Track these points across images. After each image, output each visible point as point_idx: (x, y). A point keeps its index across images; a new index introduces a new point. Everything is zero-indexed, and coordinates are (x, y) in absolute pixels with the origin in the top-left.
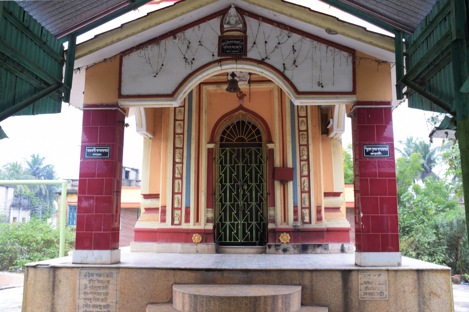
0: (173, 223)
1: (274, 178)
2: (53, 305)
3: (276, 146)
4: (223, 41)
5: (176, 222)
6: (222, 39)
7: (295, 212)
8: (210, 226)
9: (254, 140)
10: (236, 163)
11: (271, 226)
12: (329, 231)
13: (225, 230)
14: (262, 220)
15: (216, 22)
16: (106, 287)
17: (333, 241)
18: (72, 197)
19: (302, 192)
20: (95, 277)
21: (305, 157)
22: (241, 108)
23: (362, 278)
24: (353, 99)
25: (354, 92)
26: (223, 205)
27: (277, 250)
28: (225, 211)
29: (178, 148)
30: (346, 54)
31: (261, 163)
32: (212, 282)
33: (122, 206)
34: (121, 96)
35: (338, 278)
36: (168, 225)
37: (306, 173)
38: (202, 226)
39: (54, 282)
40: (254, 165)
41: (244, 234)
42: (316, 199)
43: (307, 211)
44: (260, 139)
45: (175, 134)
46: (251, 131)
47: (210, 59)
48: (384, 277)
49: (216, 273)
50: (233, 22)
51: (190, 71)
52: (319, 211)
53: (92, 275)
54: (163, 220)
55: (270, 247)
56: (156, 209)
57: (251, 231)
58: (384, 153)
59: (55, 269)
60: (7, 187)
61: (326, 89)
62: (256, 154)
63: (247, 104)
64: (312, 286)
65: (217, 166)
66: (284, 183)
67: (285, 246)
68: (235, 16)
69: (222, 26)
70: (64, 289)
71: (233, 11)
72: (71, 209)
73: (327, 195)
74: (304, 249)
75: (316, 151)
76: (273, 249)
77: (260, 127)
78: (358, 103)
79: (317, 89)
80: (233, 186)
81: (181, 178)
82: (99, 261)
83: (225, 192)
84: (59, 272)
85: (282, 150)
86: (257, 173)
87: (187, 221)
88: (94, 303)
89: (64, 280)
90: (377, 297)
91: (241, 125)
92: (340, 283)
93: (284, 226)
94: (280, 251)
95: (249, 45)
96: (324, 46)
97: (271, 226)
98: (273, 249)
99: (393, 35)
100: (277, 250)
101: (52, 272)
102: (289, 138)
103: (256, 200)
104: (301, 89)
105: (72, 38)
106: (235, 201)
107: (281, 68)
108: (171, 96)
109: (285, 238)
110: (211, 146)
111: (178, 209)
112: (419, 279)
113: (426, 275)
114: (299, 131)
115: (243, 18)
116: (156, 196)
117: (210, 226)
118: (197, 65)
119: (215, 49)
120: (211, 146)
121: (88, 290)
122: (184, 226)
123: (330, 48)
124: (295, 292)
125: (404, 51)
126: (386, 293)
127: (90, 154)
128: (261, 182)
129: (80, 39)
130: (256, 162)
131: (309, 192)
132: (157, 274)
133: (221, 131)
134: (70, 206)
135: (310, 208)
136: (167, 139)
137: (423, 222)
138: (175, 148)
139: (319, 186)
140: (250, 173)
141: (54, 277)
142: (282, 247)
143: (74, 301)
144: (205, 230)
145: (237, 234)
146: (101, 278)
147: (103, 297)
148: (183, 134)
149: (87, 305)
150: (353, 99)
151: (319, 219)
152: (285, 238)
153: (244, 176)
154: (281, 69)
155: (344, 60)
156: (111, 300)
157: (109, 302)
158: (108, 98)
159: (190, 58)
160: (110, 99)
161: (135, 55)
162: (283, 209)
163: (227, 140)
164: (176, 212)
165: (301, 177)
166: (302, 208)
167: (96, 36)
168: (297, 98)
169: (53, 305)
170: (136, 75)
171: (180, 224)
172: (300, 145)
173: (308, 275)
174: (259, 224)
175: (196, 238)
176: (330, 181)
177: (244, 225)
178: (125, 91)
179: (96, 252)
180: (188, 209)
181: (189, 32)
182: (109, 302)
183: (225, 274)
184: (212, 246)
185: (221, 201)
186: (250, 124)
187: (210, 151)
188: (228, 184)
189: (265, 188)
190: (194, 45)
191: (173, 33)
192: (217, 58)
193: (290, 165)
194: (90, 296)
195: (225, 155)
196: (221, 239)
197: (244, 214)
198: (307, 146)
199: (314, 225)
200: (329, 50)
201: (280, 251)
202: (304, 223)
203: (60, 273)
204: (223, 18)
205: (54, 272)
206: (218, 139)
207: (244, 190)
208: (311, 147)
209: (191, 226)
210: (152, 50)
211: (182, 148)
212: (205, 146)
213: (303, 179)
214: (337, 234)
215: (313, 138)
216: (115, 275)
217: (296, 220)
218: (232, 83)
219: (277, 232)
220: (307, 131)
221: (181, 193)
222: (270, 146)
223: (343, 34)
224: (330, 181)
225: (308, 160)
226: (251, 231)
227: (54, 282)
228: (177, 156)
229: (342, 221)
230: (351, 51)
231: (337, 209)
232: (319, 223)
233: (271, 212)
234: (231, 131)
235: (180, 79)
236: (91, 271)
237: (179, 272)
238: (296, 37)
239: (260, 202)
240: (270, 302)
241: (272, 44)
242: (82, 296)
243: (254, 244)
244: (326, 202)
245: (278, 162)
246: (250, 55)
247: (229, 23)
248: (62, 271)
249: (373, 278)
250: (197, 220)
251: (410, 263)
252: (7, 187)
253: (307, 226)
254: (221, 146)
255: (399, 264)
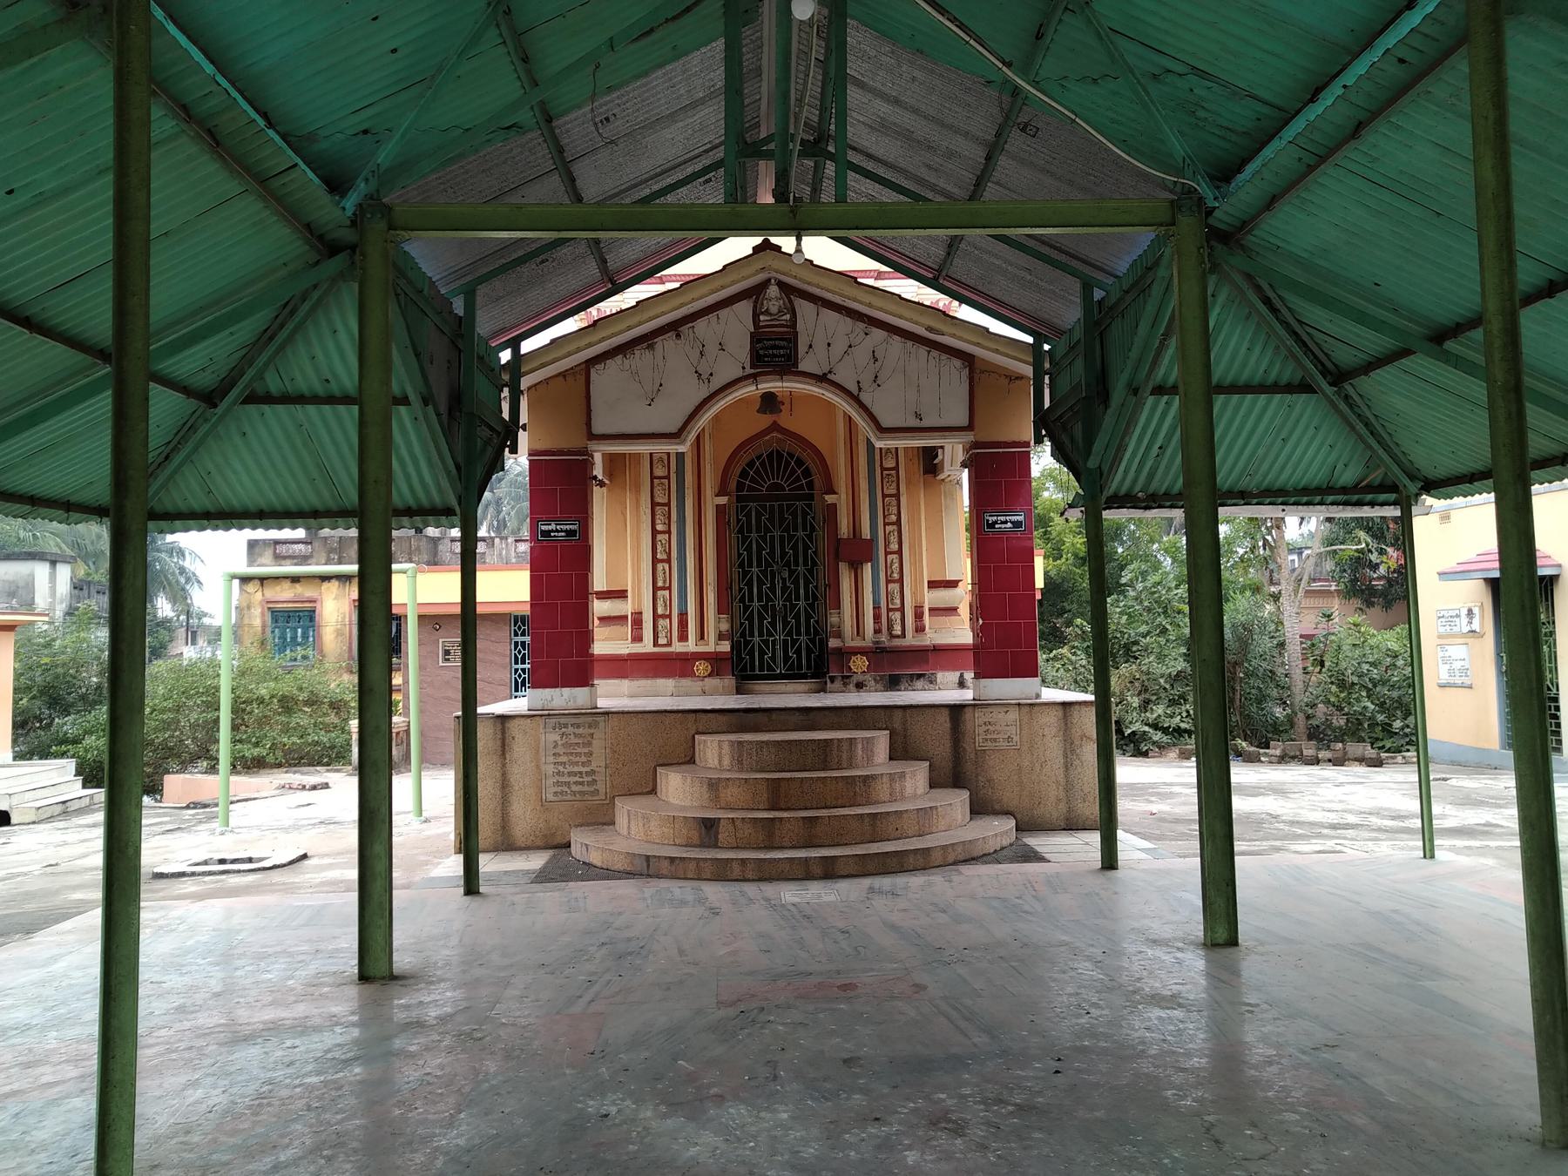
0: (656, 644)
1: (837, 558)
2: (504, 774)
3: (841, 499)
4: (759, 341)
5: (662, 641)
6: (756, 338)
7: (877, 617)
8: (725, 647)
9: (801, 487)
10: (767, 530)
11: (833, 643)
12: (937, 649)
13: (751, 653)
14: (816, 633)
15: (744, 308)
16: (589, 744)
17: (945, 668)
18: (278, 588)
19: (888, 582)
20: (570, 730)
21: (894, 518)
22: (775, 427)
23: (980, 717)
24: (970, 437)
25: (970, 427)
26: (746, 608)
27: (845, 684)
28: (750, 619)
29: (659, 504)
30: (957, 363)
31: (813, 529)
32: (756, 729)
33: (480, 610)
34: (592, 437)
35: (944, 718)
36: (647, 646)
37: (894, 547)
38: (711, 646)
39: (503, 740)
40: (801, 533)
41: (786, 658)
42: (914, 594)
43: (898, 615)
44: (810, 485)
45: (653, 478)
46: (793, 472)
47: (740, 373)
48: (1013, 715)
49: (759, 715)
50: (774, 310)
51: (704, 394)
52: (919, 615)
53: (566, 726)
54: (637, 638)
55: (832, 680)
56: (622, 619)
57: (798, 652)
58: (1017, 524)
59: (503, 719)
60: (53, 563)
61: (926, 423)
62: (805, 514)
63: (785, 420)
64: (905, 730)
65: (732, 537)
66: (856, 567)
67: (861, 678)
68: (778, 299)
69: (756, 316)
70: (520, 749)
71: (773, 291)
72: (275, 620)
73: (933, 585)
74: (893, 683)
75: (914, 506)
76: (838, 684)
77: (805, 456)
78: (976, 445)
79: (913, 422)
80: (764, 572)
81: (669, 561)
82: (571, 705)
83: (750, 584)
84: (511, 725)
85: (851, 505)
86: (806, 548)
87: (683, 637)
88: (570, 769)
89: (519, 737)
90: (1003, 744)
91: (776, 457)
92: (948, 725)
93: (858, 643)
94: (851, 686)
95: (802, 349)
96: (923, 350)
97: (833, 643)
98: (838, 684)
99: (1029, 339)
100: (845, 684)
101: (499, 726)
102: (863, 485)
103: (807, 598)
104: (885, 424)
105: (515, 344)
106: (769, 599)
107: (853, 389)
108: (676, 436)
109: (859, 664)
110: (723, 500)
111: (663, 616)
112: (1065, 716)
113: (1075, 711)
114: (883, 469)
115: (791, 301)
116: (621, 594)
117: (725, 647)
118: (717, 383)
119: (744, 354)
120: (723, 500)
121: (560, 750)
122: (678, 647)
123: (935, 353)
124: (881, 740)
125: (1047, 365)
126: (1016, 738)
127: (546, 534)
128: (814, 563)
129: (527, 346)
130: (805, 529)
131: (901, 581)
132: (669, 719)
133: (738, 471)
134: (273, 611)
135: (902, 609)
136: (637, 488)
137: (1164, 631)
138: (654, 505)
139: (919, 568)
140: (795, 548)
141: (503, 732)
142: (855, 679)
143: (538, 767)
144: (716, 653)
145: (773, 658)
146: (581, 731)
147: (584, 759)
148: (668, 477)
149: (559, 773)
150: (970, 437)
151: (920, 629)
152: (859, 664)
153: (783, 554)
154: (855, 391)
155: (954, 378)
156: (598, 763)
157: (594, 766)
158: (569, 439)
159: (704, 369)
160: (574, 441)
161: (614, 364)
162: (856, 612)
163: (751, 489)
164: (662, 623)
165: (887, 553)
166: (889, 610)
167: (553, 341)
168: (879, 439)
169: (504, 774)
170: (619, 401)
171: (669, 644)
172: (884, 496)
173: (899, 713)
174: (813, 641)
175: (701, 667)
176: (937, 561)
177: (785, 641)
178: (598, 428)
179: (567, 691)
180: (683, 616)
181: (701, 324)
182: (594, 766)
183: (774, 716)
184: (729, 681)
185: (742, 600)
186: (791, 455)
187: (720, 510)
188: (755, 569)
189: (821, 575)
190: (712, 349)
191: (674, 327)
192: (749, 371)
193: (866, 533)
194: (564, 759)
195: (748, 516)
196: (744, 669)
197: (786, 623)
198: (897, 496)
199: (911, 640)
200: (931, 360)
201: (851, 686)
202: (893, 637)
203: (513, 726)
204: (756, 302)
205: (503, 724)
206: (733, 485)
207: (784, 580)
208: (903, 500)
209: (691, 646)
210: (640, 358)
211: (668, 504)
212: (712, 501)
213: (890, 557)
214: (944, 655)
215: (908, 483)
216: (602, 724)
217: (877, 631)
218: (769, 402)
219: (844, 654)
220: (896, 468)
221: (669, 588)
222: (830, 499)
223: (953, 336)
224: (937, 561)
225: (898, 523)
226: (798, 652)
227: (503, 740)
228: (660, 519)
229: (961, 632)
230: (968, 359)
231: (953, 610)
232: (920, 636)
233: (834, 619)
234: (757, 472)
235: (691, 408)
236: (563, 721)
237: (703, 716)
238: (878, 334)
239: (813, 599)
240: (845, 746)
241: (839, 347)
242: (551, 759)
243: (804, 677)
244: (931, 598)
245: (844, 529)
246: (802, 367)
247: (767, 312)
248: (516, 722)
249: (998, 716)
250: (702, 636)
251: (1050, 694)
252: (53, 563)
253: (897, 642)
254: (739, 499)
255: (1038, 696)
